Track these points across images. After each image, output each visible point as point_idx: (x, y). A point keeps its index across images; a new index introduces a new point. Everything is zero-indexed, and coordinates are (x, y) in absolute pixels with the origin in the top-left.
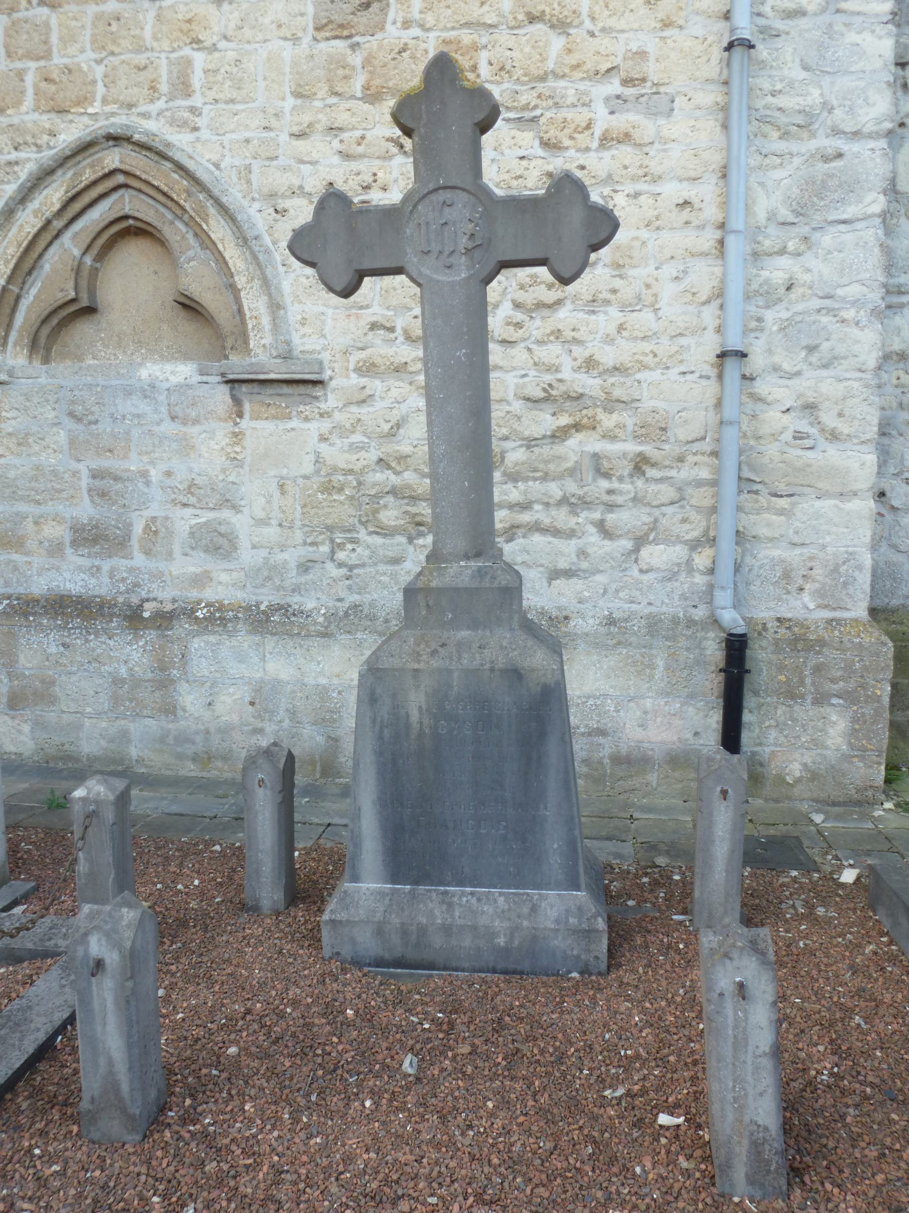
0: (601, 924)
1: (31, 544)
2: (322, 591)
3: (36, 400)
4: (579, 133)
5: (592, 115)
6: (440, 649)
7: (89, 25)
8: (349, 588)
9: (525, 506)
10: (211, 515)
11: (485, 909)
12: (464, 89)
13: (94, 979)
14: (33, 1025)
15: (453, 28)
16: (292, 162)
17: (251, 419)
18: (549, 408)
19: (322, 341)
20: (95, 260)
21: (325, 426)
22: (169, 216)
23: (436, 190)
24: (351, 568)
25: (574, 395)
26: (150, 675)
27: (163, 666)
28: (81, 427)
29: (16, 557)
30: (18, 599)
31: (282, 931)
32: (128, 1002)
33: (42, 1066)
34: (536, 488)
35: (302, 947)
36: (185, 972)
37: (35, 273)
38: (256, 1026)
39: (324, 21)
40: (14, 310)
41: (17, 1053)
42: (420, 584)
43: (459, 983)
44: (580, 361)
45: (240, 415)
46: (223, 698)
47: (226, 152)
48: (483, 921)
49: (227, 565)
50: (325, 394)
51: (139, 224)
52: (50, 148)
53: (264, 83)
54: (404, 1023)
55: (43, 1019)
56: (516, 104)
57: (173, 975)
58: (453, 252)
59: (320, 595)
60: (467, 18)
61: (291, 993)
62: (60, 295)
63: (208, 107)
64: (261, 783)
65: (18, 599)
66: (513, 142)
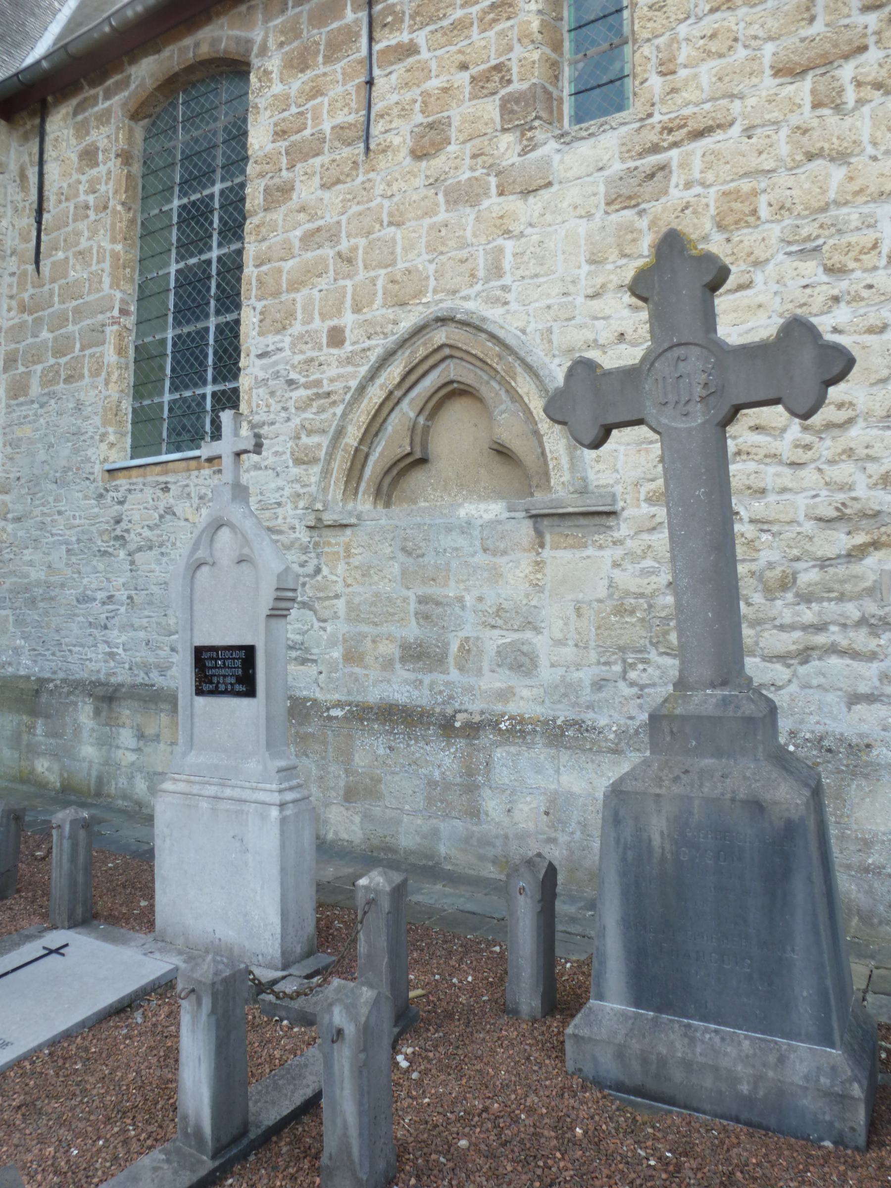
0: (857, 1091)
1: (369, 660)
2: (614, 709)
3: (377, 538)
4: (865, 254)
5: (878, 235)
6: (682, 776)
7: (424, 235)
8: (640, 707)
9: (821, 628)
10: (516, 636)
11: (729, 1050)
12: (692, 257)
13: (335, 1046)
14: (305, 1082)
15: (732, 180)
16: (588, 320)
17: (552, 549)
18: (844, 527)
19: (615, 475)
20: (427, 419)
21: (618, 552)
22: (486, 377)
23: (670, 348)
24: (642, 687)
25: (870, 512)
26: (458, 780)
27: (470, 772)
28: (411, 560)
29: (357, 670)
30: (357, 706)
31: (535, 1038)
32: (361, 1072)
33: (306, 1119)
34: (831, 609)
35: (549, 1057)
36: (440, 1061)
37: (380, 435)
38: (489, 1125)
39: (614, 197)
40: (364, 466)
41: (287, 1102)
42: (664, 711)
43: (698, 1125)
44: (875, 477)
45: (542, 545)
46: (521, 806)
47: (531, 319)
48: (725, 1063)
49: (528, 682)
50: (618, 524)
51: (462, 387)
52: (393, 334)
53: (563, 257)
54: (630, 1154)
55: (313, 1078)
56: (797, 238)
57: (430, 1061)
58: (688, 402)
59: (612, 712)
60: (746, 169)
61: (529, 1100)
62: (399, 451)
63: (517, 283)
64: (522, 890)
65: (357, 706)
66: (795, 273)
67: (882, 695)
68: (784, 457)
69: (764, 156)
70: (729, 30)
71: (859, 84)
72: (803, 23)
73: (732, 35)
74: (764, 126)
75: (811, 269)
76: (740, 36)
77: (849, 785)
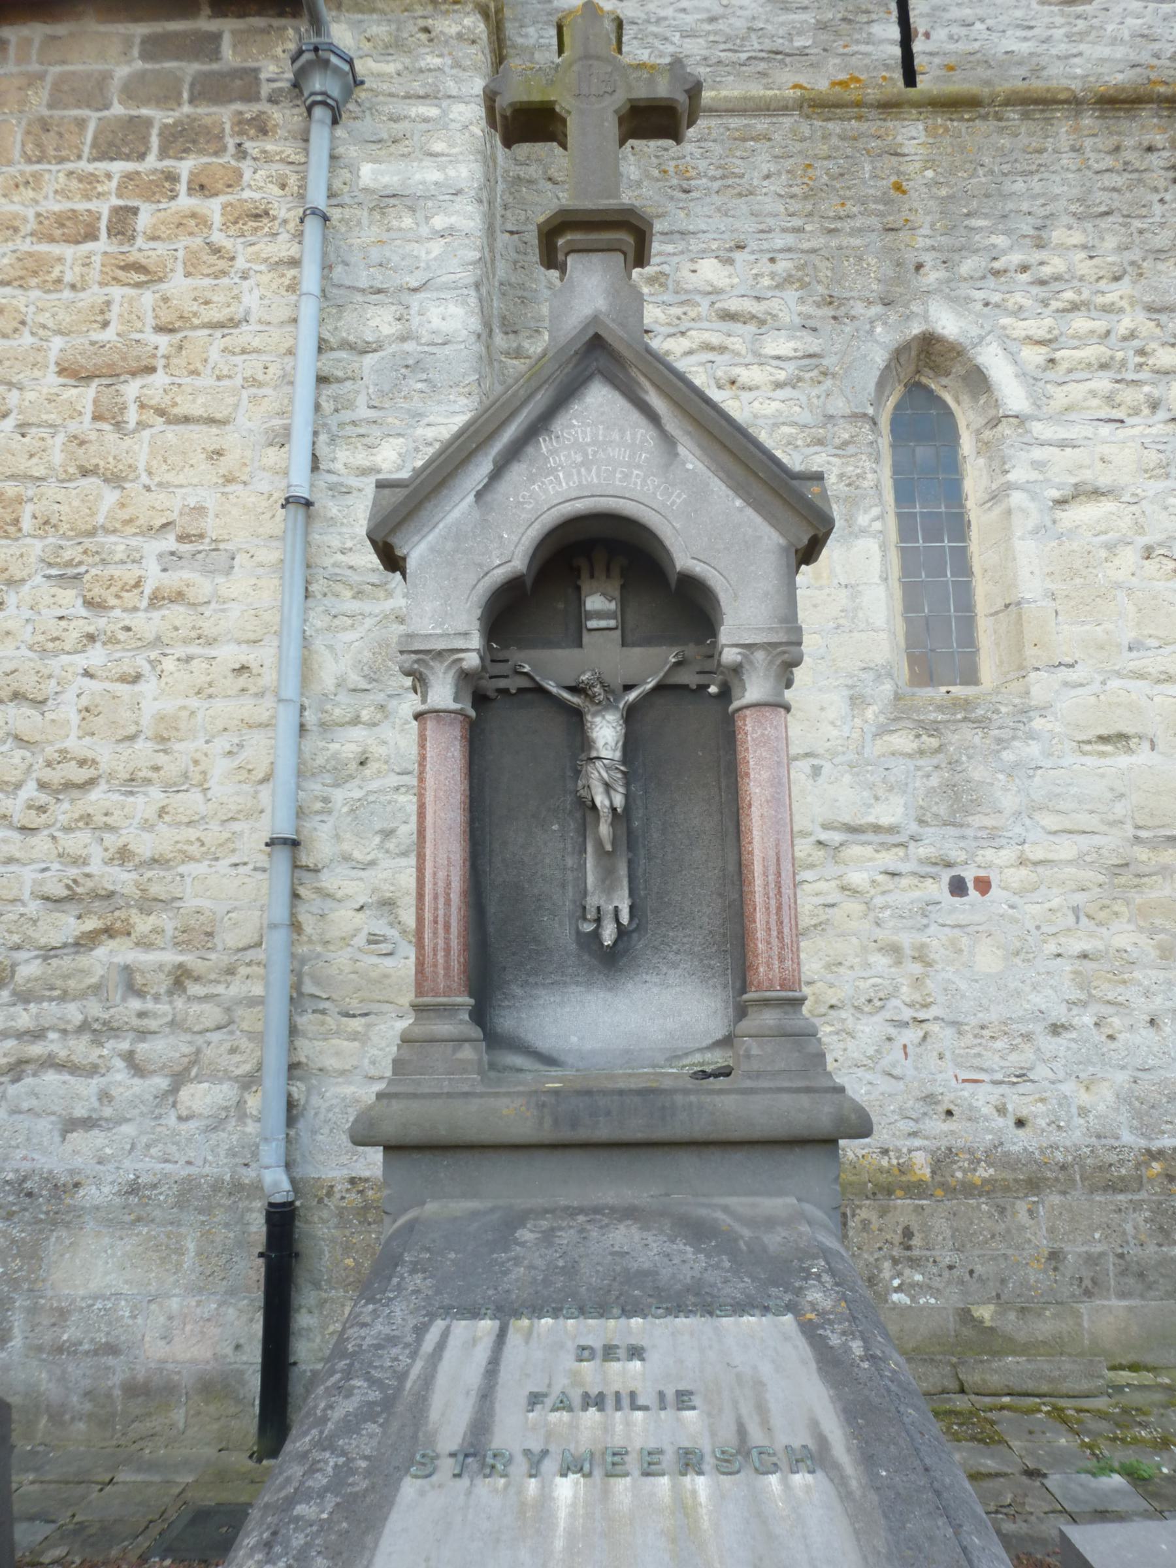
5: (142, 573)
9: (37, 1035)
18: (74, 909)
34: (51, 1010)
44: (112, 850)
60: (14, 470)
66: (52, 600)
67: (100, 1119)
68: (15, 819)
69: (35, 460)
70: (17, 311)
71: (142, 406)
72: (95, 326)
73: (20, 317)
74: (39, 426)
75: (70, 599)
76: (29, 320)
77: (47, 1239)
